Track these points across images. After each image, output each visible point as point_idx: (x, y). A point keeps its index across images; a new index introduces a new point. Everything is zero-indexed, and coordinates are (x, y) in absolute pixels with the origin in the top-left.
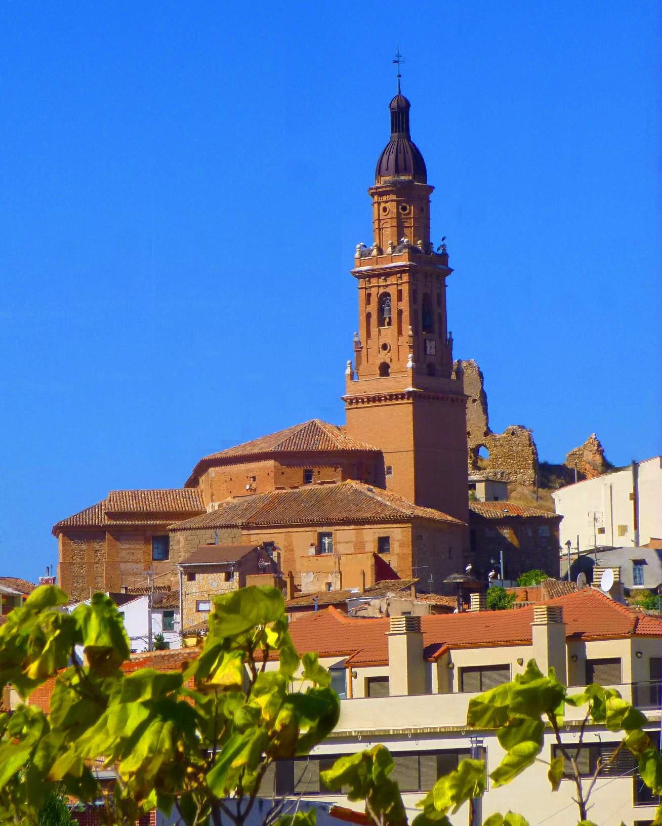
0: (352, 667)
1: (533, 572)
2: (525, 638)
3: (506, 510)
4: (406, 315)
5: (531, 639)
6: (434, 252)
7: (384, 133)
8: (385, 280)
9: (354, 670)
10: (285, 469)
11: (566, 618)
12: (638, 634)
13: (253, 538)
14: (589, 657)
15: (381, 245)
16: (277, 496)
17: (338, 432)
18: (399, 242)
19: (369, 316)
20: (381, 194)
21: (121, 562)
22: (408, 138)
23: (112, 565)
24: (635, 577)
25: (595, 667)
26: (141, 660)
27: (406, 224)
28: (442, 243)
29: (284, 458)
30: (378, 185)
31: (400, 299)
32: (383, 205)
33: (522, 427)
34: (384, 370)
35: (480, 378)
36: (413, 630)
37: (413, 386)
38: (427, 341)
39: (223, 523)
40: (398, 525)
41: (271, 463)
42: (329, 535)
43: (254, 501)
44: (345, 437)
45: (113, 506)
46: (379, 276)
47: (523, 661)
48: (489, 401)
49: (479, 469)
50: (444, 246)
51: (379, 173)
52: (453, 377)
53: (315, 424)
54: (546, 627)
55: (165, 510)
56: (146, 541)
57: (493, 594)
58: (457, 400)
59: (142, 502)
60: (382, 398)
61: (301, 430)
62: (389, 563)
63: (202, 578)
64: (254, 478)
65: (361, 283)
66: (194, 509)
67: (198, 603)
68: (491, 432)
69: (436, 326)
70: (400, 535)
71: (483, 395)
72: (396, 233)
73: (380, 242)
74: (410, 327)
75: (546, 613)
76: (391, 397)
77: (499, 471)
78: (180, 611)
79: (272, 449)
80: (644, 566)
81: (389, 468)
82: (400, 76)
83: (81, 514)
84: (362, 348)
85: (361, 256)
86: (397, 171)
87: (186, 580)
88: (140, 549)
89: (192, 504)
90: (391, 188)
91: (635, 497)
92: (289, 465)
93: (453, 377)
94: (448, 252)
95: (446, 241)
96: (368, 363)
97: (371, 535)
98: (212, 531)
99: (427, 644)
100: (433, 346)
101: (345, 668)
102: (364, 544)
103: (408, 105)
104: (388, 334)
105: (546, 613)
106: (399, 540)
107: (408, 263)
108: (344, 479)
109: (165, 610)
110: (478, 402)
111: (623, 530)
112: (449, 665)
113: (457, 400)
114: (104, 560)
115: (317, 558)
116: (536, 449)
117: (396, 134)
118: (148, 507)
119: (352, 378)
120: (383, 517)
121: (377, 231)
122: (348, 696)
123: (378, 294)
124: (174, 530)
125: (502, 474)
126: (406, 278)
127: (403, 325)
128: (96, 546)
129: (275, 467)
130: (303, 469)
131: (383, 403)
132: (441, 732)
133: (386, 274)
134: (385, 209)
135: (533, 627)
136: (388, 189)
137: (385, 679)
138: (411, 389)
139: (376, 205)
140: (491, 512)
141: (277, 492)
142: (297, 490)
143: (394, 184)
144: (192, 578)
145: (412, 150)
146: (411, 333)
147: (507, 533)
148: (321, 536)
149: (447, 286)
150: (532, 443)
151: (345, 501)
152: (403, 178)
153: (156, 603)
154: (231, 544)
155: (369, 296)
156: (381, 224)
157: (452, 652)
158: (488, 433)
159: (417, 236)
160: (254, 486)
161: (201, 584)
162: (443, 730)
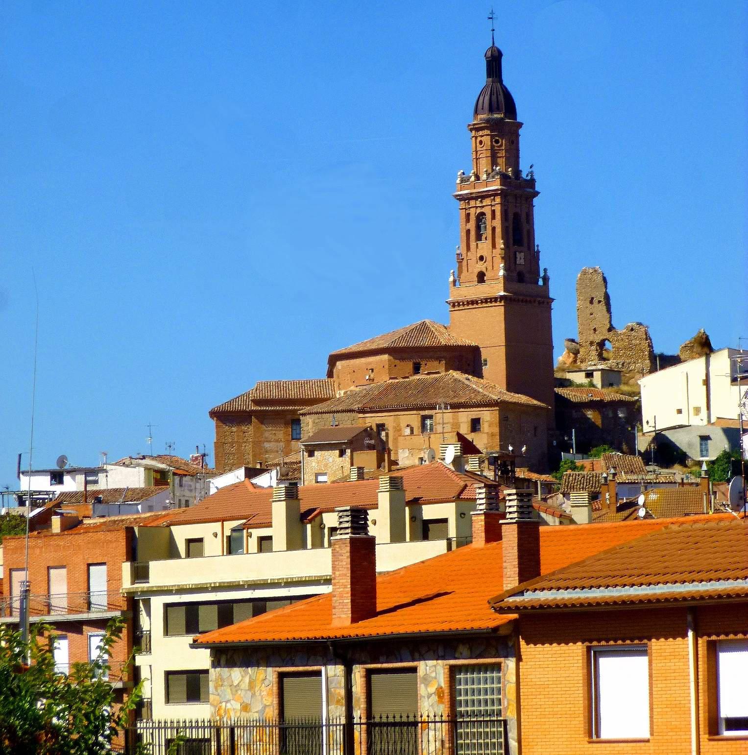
0: (248, 529)
1: (601, 448)
2: (373, 503)
3: (590, 395)
4: (499, 231)
5: (377, 504)
6: (522, 178)
7: (480, 79)
8: (481, 202)
9: (250, 530)
10: (397, 362)
11: (406, 485)
12: (462, 498)
13: (368, 420)
14: (425, 518)
15: (478, 173)
16: (392, 384)
17: (445, 331)
18: (493, 170)
19: (468, 232)
20: (477, 130)
21: (265, 442)
22: (501, 81)
23: (257, 444)
24: (701, 451)
25: (430, 526)
26: (98, 524)
27: (499, 155)
28: (530, 170)
29: (397, 352)
30: (475, 122)
31: (493, 217)
32: (479, 139)
33: (640, 324)
34: (481, 277)
35: (604, 283)
36: (292, 498)
37: (504, 291)
38: (517, 253)
39: (344, 408)
40: (487, 409)
41: (386, 357)
42: (431, 417)
43: (371, 390)
44: (449, 335)
45: (258, 394)
46: (476, 198)
47: (376, 522)
48: (612, 302)
49: (604, 359)
50: (532, 173)
51: (476, 112)
52: (541, 283)
53: (426, 324)
54: (388, 493)
55: (301, 397)
56: (286, 424)
57: (566, 466)
58: (543, 302)
59: (283, 390)
60: (479, 302)
61: (413, 329)
62: (473, 440)
63: (320, 454)
64: (372, 370)
65: (462, 204)
66: (326, 397)
67: (317, 475)
68: (614, 328)
69: (525, 241)
70: (489, 417)
71: (607, 297)
72: (490, 162)
73: (477, 171)
74: (502, 241)
75: (388, 482)
76: (486, 301)
77: (621, 361)
78: (302, 482)
79: (386, 345)
80: (709, 441)
81: (485, 361)
82: (493, 30)
83: (232, 402)
84: (463, 259)
85: (462, 181)
86: (491, 110)
87: (307, 456)
88: (281, 430)
89: (325, 392)
90: (485, 125)
91: (707, 382)
92: (402, 359)
93: (541, 283)
94: (535, 177)
95: (533, 169)
96: (468, 272)
97: (465, 417)
98: (331, 415)
99: (303, 510)
100: (523, 257)
101: (243, 529)
102: (460, 425)
103: (500, 54)
104: (484, 247)
105: (388, 482)
106: (488, 421)
107: (500, 187)
108: (447, 370)
109: (291, 481)
110: (603, 303)
111: (697, 410)
112: (321, 526)
113: (543, 302)
114: (251, 440)
115: (411, 437)
116: (651, 343)
117: (491, 79)
118: (288, 395)
119: (455, 285)
120: (475, 402)
121: (475, 160)
122: (245, 552)
123: (476, 213)
124: (303, 414)
125: (623, 364)
126: (498, 200)
127: (471, 243)
128: (244, 428)
129: (389, 360)
130: (412, 361)
131: (480, 305)
132: (305, 581)
133: (483, 196)
134: (481, 142)
135: (379, 494)
136: (483, 125)
137: (270, 538)
138: (502, 293)
139: (474, 139)
140: (577, 397)
141: (391, 381)
142: (408, 380)
143: (488, 121)
144: (311, 454)
145: (503, 91)
146: (502, 246)
147: (590, 414)
148: (424, 418)
149: (534, 206)
150: (648, 338)
151: (446, 389)
152: (495, 116)
153: (283, 476)
154: (349, 426)
155: (468, 215)
156: (478, 154)
157: (324, 515)
158: (611, 329)
159: (508, 165)
160: (372, 376)
161: (319, 459)
162: (307, 579)
